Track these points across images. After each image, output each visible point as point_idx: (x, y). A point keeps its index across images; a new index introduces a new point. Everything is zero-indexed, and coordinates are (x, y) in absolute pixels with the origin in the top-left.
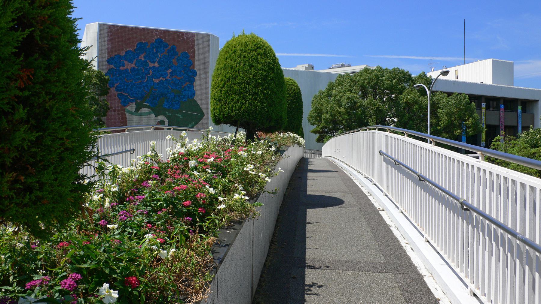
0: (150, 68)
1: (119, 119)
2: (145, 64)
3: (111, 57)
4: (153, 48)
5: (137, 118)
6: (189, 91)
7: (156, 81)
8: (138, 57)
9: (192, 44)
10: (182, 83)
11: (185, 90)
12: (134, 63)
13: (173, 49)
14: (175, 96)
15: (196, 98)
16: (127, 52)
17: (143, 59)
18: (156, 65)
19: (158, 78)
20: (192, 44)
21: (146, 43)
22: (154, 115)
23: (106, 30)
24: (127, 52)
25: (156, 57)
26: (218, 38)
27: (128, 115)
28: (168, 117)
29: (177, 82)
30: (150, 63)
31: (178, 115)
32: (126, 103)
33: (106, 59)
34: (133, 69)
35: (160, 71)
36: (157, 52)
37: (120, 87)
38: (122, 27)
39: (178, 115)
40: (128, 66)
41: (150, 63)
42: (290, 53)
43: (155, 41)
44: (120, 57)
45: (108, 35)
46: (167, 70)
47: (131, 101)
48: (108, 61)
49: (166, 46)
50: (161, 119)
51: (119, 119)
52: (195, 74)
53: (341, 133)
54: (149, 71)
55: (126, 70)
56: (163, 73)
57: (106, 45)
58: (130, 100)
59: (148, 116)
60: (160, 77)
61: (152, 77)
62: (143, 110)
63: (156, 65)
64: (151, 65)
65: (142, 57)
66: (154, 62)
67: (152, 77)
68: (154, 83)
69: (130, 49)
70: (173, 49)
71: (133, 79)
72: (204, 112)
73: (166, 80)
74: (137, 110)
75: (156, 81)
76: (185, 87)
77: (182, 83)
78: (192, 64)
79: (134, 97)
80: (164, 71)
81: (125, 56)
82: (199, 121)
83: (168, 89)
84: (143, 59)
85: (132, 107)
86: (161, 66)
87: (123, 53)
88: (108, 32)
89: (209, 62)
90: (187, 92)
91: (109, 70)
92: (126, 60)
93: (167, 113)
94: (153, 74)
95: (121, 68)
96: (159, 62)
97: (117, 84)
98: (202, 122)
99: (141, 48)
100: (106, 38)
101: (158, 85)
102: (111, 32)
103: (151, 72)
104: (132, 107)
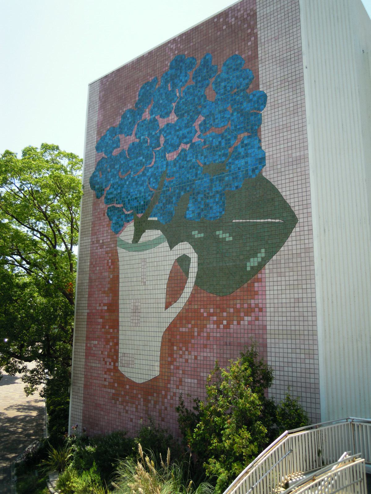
5: (137, 256)
7: (171, 156)
15: (268, 173)
18: (173, 118)
29: (215, 143)
30: (160, 120)
31: (220, 234)
39: (220, 234)
42: (276, 438)
48: (97, 148)
51: (108, 263)
54: (158, 139)
56: (185, 131)
58: (127, 216)
60: (179, 146)
62: (150, 235)
66: (168, 114)
67: (165, 150)
72: (296, 210)
73: (193, 146)
75: (171, 156)
78: (254, 79)
80: (187, 126)
82: (282, 242)
90: (242, 162)
98: (291, 244)
100: (97, 107)
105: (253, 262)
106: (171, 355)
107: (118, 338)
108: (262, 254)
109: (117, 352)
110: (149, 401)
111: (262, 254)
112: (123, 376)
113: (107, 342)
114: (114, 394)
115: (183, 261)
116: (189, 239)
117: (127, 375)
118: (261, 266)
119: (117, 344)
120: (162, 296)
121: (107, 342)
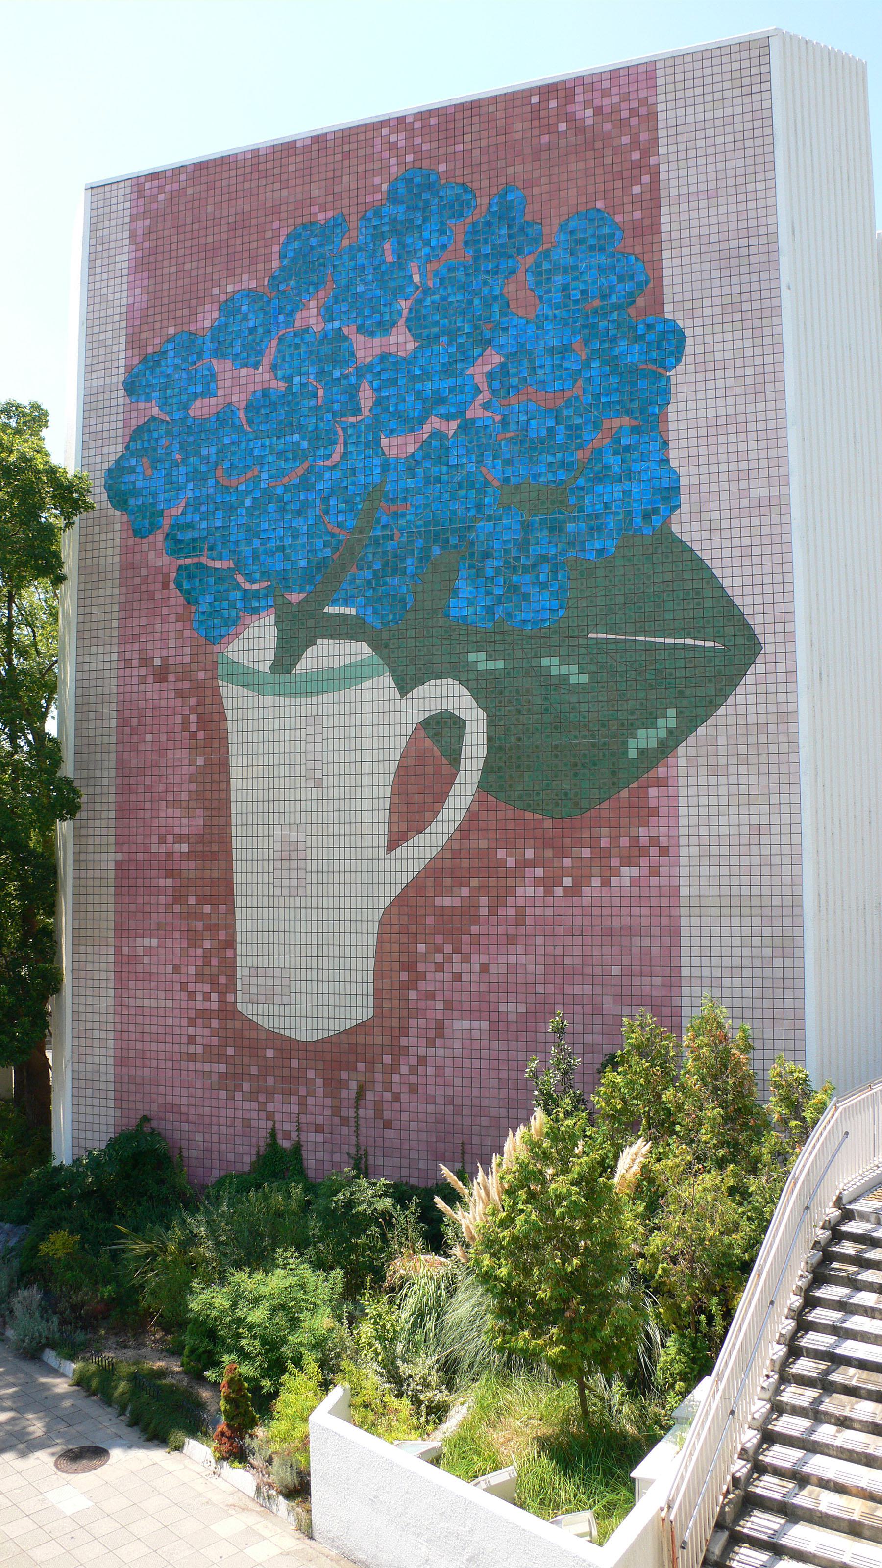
0: (361, 373)
1: (186, 723)
2: (332, 351)
3: (144, 360)
4: (379, 236)
5: (288, 709)
6: (628, 475)
7: (398, 446)
8: (289, 323)
9: (635, 143)
10: (574, 431)
11: (599, 479)
12: (266, 361)
13: (505, 213)
14: (526, 527)
15: (685, 526)
16: (229, 308)
17: (316, 324)
18: (401, 341)
19: (410, 424)
20: (635, 143)
21: (339, 223)
22: (387, 680)
23: (123, 208)
24: (229, 308)
25: (398, 292)
26: (864, 67)
27: (233, 695)
28: (484, 690)
30: (359, 341)
31: (553, 664)
32: (220, 624)
33: (119, 375)
34: (261, 404)
35: (426, 376)
36: (404, 254)
37: (190, 526)
38: (202, 167)
39: (553, 664)
40: (237, 384)
41: (359, 341)
43: (393, 197)
44: (189, 345)
45: (133, 236)
46: (467, 359)
47: (252, 606)
49: (458, 208)
50: (434, 707)
51: (186, 723)
52: (672, 342)
53: (164, 1139)
54: (352, 393)
55: (224, 417)
56: (445, 385)
57: (120, 296)
59: (351, 694)
60: (422, 420)
61: (376, 426)
62: (324, 654)
63: (401, 341)
64: (366, 348)
65: (310, 317)
66: (385, 327)
67: (376, 426)
68: (385, 467)
69: (248, 282)
70: (505, 213)
71: (260, 461)
72: (757, 622)
73: (466, 427)
74: (287, 655)
75: (398, 446)
76: (598, 453)
77: (574, 431)
78: (651, 286)
79: (266, 574)
80: (447, 371)
81: (218, 330)
83: (482, 491)
84: (316, 324)
85: (256, 641)
86: (428, 341)
87: (208, 318)
88: (134, 219)
89: (773, 237)
90: (615, 491)
91: (137, 434)
92: (219, 353)
93: (480, 660)
94: (379, 402)
95: (199, 408)
96: (416, 322)
97: (177, 511)
98: (744, 698)
99: (306, 265)
100: (123, 260)
101: (411, 471)
102: (144, 215)
103: (366, 397)
104: (256, 641)
105: (647, 739)
106: (410, 966)
107: (231, 929)
108: (670, 719)
109: (230, 967)
110: (343, 1085)
111: (670, 719)
112: (256, 1026)
113: (193, 939)
114: (223, 1076)
115: (443, 729)
116: (458, 670)
117: (266, 1023)
118: (666, 748)
119: (231, 944)
120: (378, 820)
121: (193, 939)
